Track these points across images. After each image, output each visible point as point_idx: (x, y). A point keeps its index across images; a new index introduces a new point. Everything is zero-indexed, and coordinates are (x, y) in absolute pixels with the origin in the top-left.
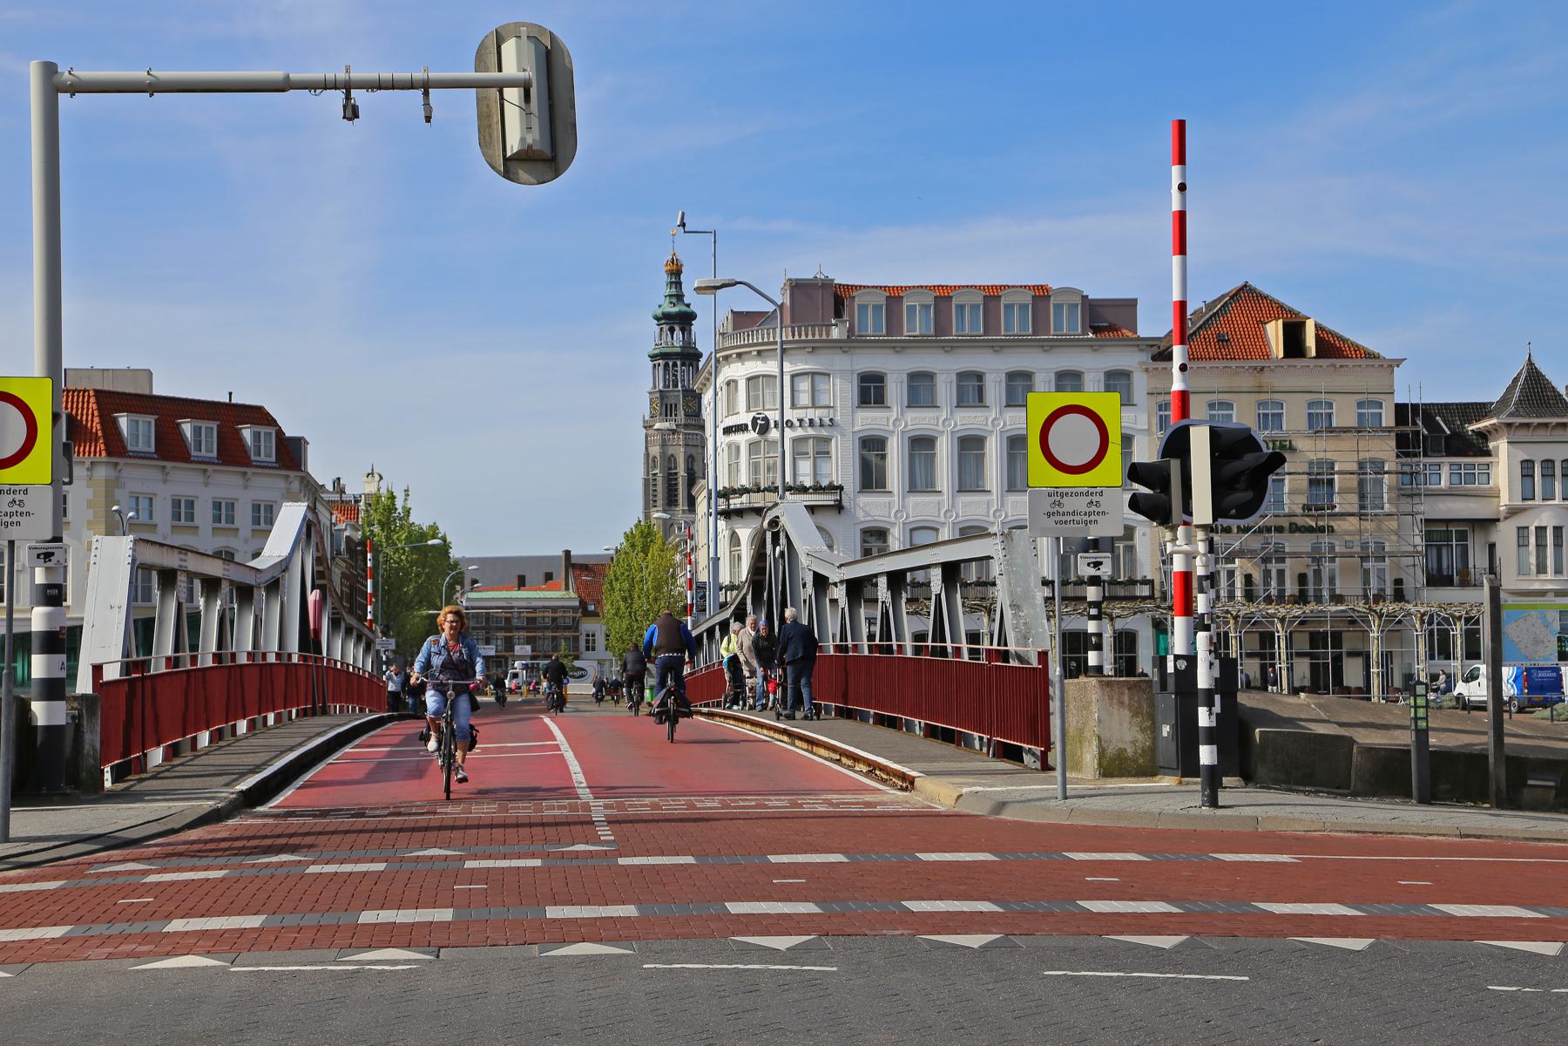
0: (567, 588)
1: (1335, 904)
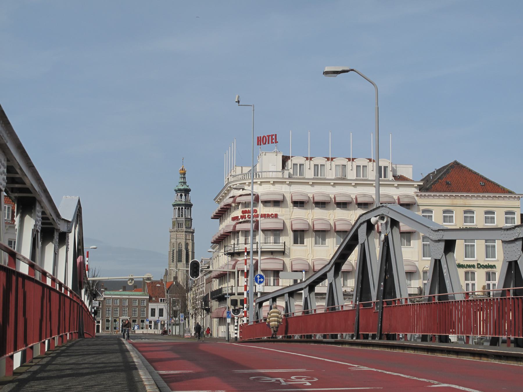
0: (144, 291)
1: (40, 317)
